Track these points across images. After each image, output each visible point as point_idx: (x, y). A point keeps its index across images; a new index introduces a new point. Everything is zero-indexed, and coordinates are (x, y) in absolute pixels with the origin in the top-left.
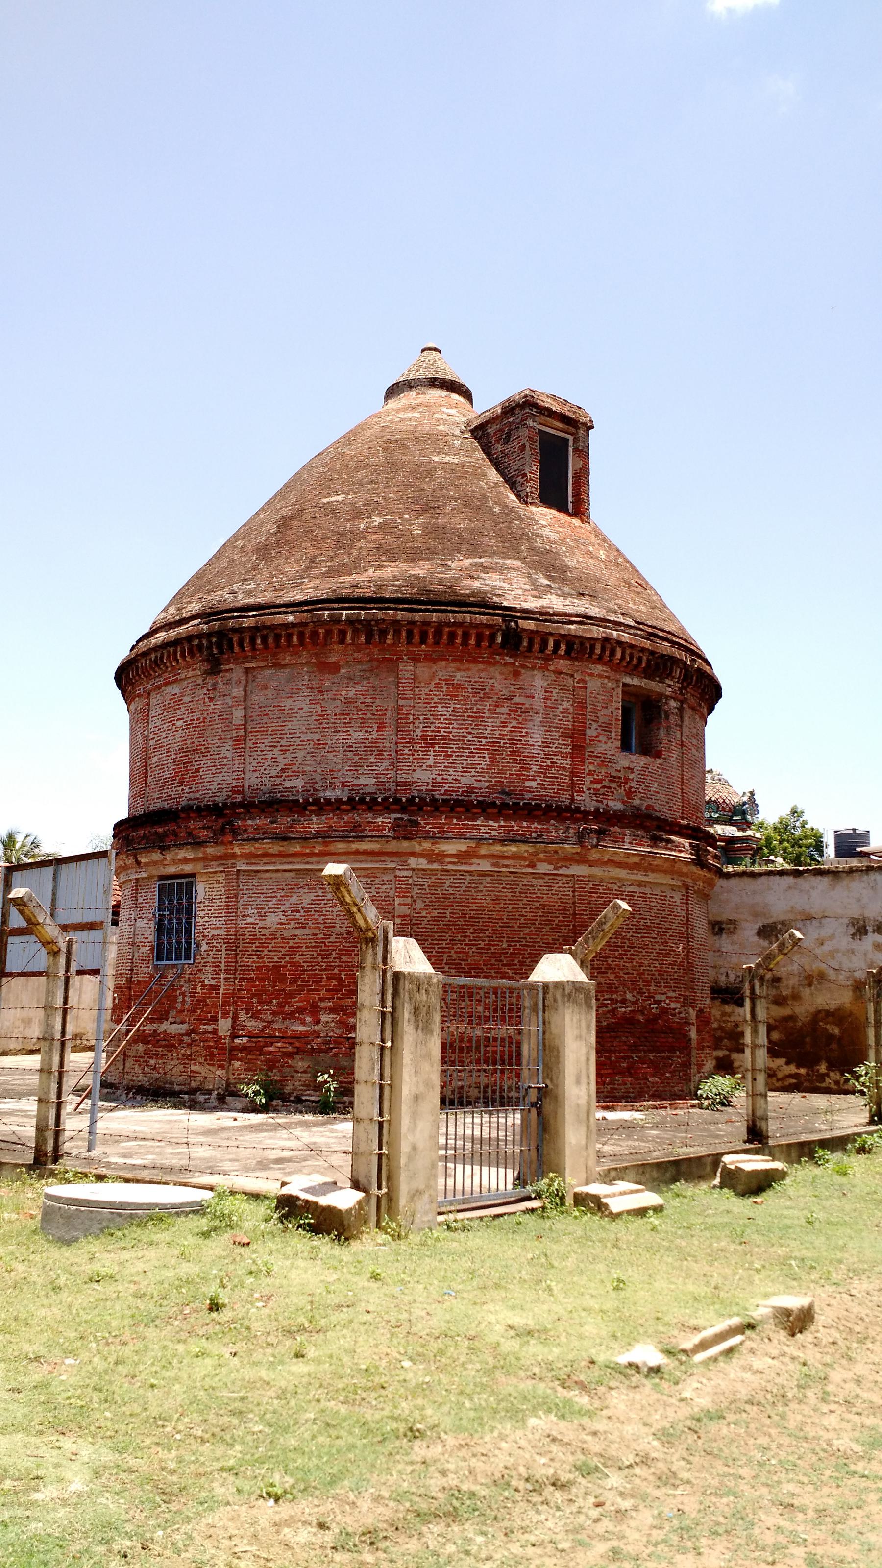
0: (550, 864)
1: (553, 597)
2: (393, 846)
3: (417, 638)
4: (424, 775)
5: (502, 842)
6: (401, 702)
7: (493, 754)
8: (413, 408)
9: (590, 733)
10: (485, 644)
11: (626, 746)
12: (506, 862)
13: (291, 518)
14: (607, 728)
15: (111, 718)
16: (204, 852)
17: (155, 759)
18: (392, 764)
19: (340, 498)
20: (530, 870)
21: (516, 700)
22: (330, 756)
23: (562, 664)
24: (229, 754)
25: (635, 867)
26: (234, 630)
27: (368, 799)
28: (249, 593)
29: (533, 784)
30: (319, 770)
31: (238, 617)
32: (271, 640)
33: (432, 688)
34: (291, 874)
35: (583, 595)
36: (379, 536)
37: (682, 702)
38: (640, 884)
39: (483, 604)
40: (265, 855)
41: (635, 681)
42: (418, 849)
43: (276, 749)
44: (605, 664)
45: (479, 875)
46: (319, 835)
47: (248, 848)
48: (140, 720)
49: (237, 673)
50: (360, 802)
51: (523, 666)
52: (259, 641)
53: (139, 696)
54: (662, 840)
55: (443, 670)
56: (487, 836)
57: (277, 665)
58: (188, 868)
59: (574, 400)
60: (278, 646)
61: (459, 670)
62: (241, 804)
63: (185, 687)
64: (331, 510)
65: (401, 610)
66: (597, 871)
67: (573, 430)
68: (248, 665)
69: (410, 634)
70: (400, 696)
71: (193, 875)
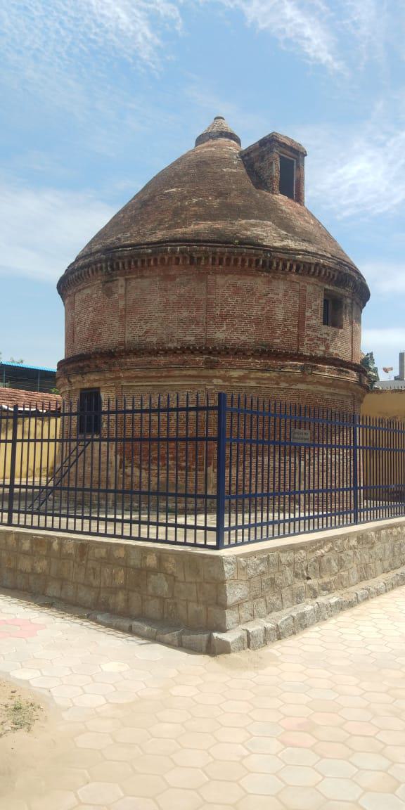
0: (287, 382)
1: (290, 241)
2: (205, 373)
3: (217, 262)
4: (220, 335)
5: (262, 371)
6: (209, 296)
7: (257, 324)
8: (212, 146)
9: (308, 314)
10: (253, 265)
11: (325, 322)
12: (264, 382)
13: (149, 201)
14: (316, 311)
15: (56, 310)
16: (105, 376)
17: (78, 328)
18: (204, 329)
19: (174, 190)
20: (276, 386)
21: (270, 296)
22: (171, 325)
23: (294, 277)
24: (117, 324)
25: (329, 385)
26: (119, 258)
27: (191, 348)
28: (127, 238)
29: (278, 341)
30: (165, 332)
31: (121, 251)
32: (139, 263)
33: (224, 287)
34: (150, 388)
35: (305, 240)
36: (196, 208)
37: (353, 300)
38: (332, 394)
39: (254, 244)
40: (136, 377)
41: (330, 288)
42: (218, 374)
43: (142, 322)
44: (315, 277)
45: (250, 389)
46: (165, 366)
47: (127, 374)
48: (70, 307)
49: (121, 281)
50: (186, 349)
51: (273, 278)
52: (133, 264)
53: (70, 296)
54: (343, 371)
55: (230, 279)
56: (254, 368)
57: (142, 277)
58: (96, 385)
59: (297, 140)
60: (143, 266)
61: (239, 279)
62: (124, 351)
63: (92, 291)
64: (169, 196)
65: (209, 246)
66: (310, 387)
67: (297, 157)
68: (127, 277)
69: (214, 259)
70: (208, 293)
71: (99, 388)
